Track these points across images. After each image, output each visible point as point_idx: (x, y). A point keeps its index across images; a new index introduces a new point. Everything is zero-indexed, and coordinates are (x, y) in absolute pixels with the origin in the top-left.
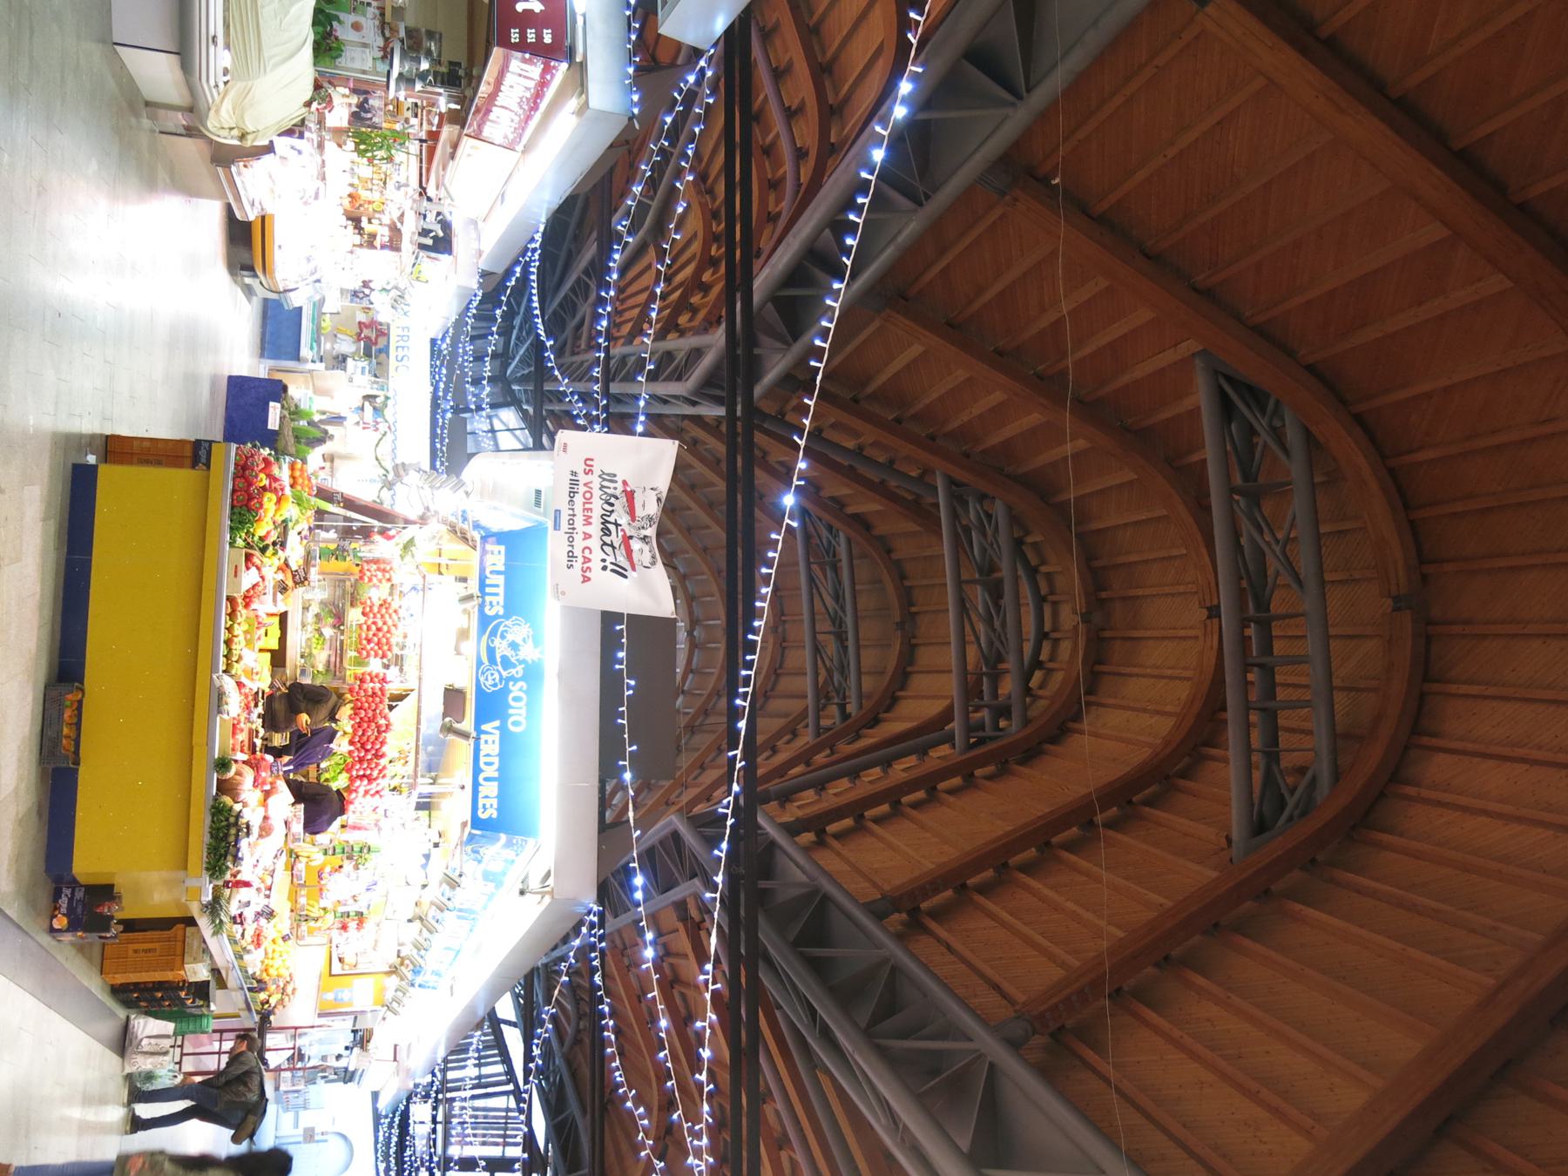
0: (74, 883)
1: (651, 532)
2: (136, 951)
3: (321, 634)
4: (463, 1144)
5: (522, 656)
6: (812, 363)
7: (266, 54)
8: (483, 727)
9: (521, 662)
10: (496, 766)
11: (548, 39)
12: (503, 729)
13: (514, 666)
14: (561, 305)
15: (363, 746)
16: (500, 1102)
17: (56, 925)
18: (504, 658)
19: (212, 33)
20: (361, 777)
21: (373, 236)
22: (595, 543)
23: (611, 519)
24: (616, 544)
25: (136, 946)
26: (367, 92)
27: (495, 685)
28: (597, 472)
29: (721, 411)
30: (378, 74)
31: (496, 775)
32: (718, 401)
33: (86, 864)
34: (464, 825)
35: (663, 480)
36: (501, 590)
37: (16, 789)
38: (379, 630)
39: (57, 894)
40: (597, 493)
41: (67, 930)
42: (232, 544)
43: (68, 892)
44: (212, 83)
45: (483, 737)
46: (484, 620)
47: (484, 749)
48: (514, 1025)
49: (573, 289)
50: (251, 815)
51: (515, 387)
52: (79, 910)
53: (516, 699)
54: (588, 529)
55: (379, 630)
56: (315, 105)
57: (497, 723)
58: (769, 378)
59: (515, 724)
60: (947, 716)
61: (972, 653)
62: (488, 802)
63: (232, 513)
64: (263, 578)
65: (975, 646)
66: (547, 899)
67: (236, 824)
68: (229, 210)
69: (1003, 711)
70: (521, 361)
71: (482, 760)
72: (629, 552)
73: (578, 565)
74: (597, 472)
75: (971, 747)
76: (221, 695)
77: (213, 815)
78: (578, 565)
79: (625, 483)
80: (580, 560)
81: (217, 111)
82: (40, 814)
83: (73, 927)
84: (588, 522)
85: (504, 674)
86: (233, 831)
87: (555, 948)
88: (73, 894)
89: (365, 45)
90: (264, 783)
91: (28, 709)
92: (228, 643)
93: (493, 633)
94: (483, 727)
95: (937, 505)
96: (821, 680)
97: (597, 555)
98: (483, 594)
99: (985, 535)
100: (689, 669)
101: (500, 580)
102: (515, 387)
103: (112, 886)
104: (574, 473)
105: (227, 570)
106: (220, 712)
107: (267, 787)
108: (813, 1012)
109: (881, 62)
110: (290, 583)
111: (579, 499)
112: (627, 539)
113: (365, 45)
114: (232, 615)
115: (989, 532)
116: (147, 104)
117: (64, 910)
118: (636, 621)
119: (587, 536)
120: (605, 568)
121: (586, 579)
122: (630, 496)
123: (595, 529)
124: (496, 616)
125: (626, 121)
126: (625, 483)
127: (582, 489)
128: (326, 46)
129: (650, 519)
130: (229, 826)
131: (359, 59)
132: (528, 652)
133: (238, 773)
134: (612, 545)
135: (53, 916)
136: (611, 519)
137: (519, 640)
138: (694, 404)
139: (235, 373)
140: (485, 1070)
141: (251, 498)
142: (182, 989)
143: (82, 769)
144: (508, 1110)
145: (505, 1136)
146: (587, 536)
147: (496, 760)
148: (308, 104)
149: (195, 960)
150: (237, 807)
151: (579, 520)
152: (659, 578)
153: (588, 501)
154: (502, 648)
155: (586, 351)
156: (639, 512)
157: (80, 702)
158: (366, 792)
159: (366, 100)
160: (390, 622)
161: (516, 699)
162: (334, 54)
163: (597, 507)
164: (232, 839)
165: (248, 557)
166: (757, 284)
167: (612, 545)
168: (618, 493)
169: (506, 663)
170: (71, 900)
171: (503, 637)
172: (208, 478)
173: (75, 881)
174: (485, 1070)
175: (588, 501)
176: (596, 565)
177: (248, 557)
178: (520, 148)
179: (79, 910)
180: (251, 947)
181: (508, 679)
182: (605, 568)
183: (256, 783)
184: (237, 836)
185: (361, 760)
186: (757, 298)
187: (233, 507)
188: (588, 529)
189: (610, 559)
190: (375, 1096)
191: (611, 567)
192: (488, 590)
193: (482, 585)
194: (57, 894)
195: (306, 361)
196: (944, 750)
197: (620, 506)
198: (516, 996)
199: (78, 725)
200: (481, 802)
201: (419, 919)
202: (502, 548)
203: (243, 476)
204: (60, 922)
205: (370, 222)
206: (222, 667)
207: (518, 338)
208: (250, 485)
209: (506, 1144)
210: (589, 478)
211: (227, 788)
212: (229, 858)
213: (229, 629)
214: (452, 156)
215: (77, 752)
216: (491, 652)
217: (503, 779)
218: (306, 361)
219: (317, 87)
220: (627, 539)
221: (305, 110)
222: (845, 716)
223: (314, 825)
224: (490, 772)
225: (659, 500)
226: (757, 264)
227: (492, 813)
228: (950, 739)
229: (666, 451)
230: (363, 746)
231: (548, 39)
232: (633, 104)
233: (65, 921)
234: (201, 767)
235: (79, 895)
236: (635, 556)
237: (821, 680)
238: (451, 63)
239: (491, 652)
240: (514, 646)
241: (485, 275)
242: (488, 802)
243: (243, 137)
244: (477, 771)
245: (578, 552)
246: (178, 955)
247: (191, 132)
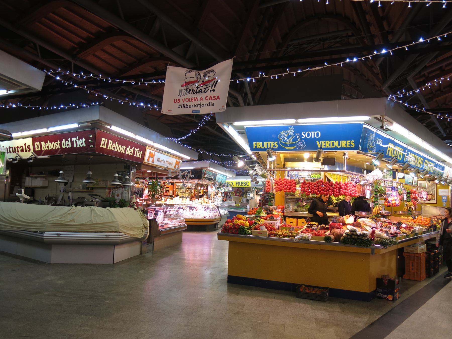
0: (375, 292)
1: (202, 73)
2: (412, 269)
3: (305, 205)
5: (292, 134)
7: (111, 221)
8: (319, 147)
9: (295, 134)
10: (334, 142)
11: (91, 136)
12: (320, 140)
15: (328, 190)
17: (392, 299)
18: (293, 141)
19: (105, 236)
20: (340, 191)
21: (204, 192)
22: (204, 95)
23: (195, 90)
24: (205, 87)
25: (411, 269)
27: (303, 143)
28: (179, 97)
30: (129, 189)
31: (337, 142)
33: (366, 287)
34: (358, 153)
35: (182, 71)
36: (269, 143)
37: (329, 312)
38: (286, 185)
39: (380, 298)
40: (186, 97)
41: (393, 295)
42: (250, 234)
43: (379, 294)
44: (121, 236)
45: (323, 147)
46: (280, 148)
50: (347, 229)
52: (386, 291)
54: (199, 99)
55: (286, 185)
56: (136, 207)
57: (318, 142)
59: (318, 134)
62: (348, 144)
63: (240, 234)
64: (264, 224)
66: (386, 117)
67: (350, 235)
68: (184, 231)
72: (209, 81)
73: (213, 102)
74: (179, 97)
76: (302, 239)
77: (346, 244)
78: (213, 102)
79: (182, 86)
80: (210, 101)
81: (133, 235)
82: (344, 303)
83: (392, 293)
84: (196, 99)
85: (299, 140)
86: (353, 237)
88: (380, 292)
89: (122, 193)
90: (339, 225)
91: (301, 305)
92: (284, 236)
93: (284, 145)
94: (319, 147)
97: (208, 94)
98: (268, 149)
101: (265, 143)
103: (378, 280)
104: (179, 106)
105: (260, 236)
106: (308, 240)
107: (341, 224)
109: (129, 40)
110: (270, 215)
111: (189, 104)
112: (204, 83)
113: (122, 193)
114: (275, 235)
116: (141, 254)
117: (385, 296)
118: (234, 75)
119: (201, 99)
120: (214, 90)
121: (218, 98)
122: (187, 83)
123: (199, 96)
124: (278, 144)
125: (102, 107)
126: (182, 86)
127: (185, 103)
128: (122, 204)
129: (197, 75)
130: (351, 238)
131: (126, 195)
132: (291, 132)
133: (333, 234)
134: (205, 89)
135: (388, 299)
136: (195, 90)
137: (286, 135)
141: (235, 228)
142: (430, 254)
143: (330, 287)
146: (201, 99)
147: (331, 142)
148: (136, 209)
149: (417, 249)
150: (344, 235)
151: (196, 103)
152: (218, 67)
153: (189, 100)
154: (289, 142)
156: (194, 79)
157: (306, 286)
158: (346, 189)
159: (136, 192)
160: (283, 182)
162: (123, 202)
163: (191, 96)
164: (356, 237)
165: (256, 229)
167: (205, 89)
168: (186, 88)
169: (295, 140)
170: (382, 293)
171: (286, 141)
173: (374, 291)
175: (189, 100)
176: (212, 94)
177: (256, 229)
179: (386, 291)
180: (412, 230)
181: (301, 139)
182: (214, 90)
183: (339, 228)
184: (355, 235)
185: (333, 191)
187: (238, 234)
188: (199, 99)
189: (210, 89)
191: (213, 88)
194: (380, 298)
195: (247, 211)
197: (190, 87)
199: (314, 287)
200: (348, 146)
201: (404, 169)
202: (254, 143)
203: (228, 230)
204: (390, 297)
205: (200, 193)
206: (293, 239)
208: (231, 228)
210: (181, 101)
211: (338, 237)
212: (363, 238)
213: (280, 236)
215: (324, 288)
216: (291, 145)
217: (339, 139)
218: (247, 211)
219: (131, 206)
220: (204, 83)
221: (138, 210)
222: (353, 35)
223: (368, 209)
224: (336, 143)
225: (190, 72)
227: (352, 142)
229: (171, 71)
230: (328, 190)
231: (91, 136)
232: (99, 104)
233: (390, 296)
234: (328, 247)
235: (380, 290)
236: (210, 79)
238: (124, 168)
239: (291, 145)
240: (289, 137)
242: (348, 144)
243: (146, 228)
244: (336, 148)
245: (207, 102)
246: (416, 256)
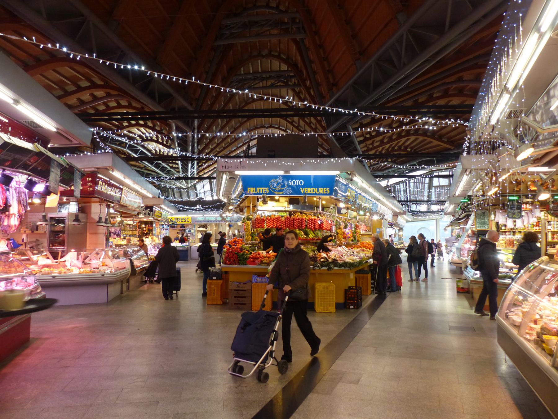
4: (423, 196)
6: (115, 67)
11: (90, 179)
14: (163, 172)
16: (412, 184)
18: (281, 187)
26: (110, 233)
29: (196, 120)
32: (193, 122)
36: (261, 189)
47: (309, 192)
48: (388, 181)
49: (158, 168)
53: (294, 183)
58: (185, 104)
59: (301, 183)
60: (295, 41)
61: (275, 32)
62: (325, 191)
65: (272, 31)
69: (293, 20)
71: (312, 193)
75: (305, 32)
93: (274, 190)
95: (223, 45)
96: (282, 84)
99: (233, 27)
100: (285, 131)
101: (258, 189)
108: (391, 87)
115: (232, 26)
124: (269, 189)
137: (276, 183)
138: (194, 128)
139: (181, 272)
140: (402, 189)
144: (414, 182)
145: (422, 183)
154: (278, 188)
166: (156, 110)
171: (275, 187)
172: (232, 272)
174: (402, 189)
178: (121, 187)
186: (161, 109)
190: (407, 222)
193: (260, 194)
196: (307, 42)
198: (380, 181)
209: (425, 183)
214: (126, 207)
216: (280, 191)
226: (147, 110)
228: (302, 40)
231: (90, 179)
237: (282, 84)
239: (280, 191)
240: (278, 184)
241: (10, 206)
242: (325, 191)
247: (128, 281)
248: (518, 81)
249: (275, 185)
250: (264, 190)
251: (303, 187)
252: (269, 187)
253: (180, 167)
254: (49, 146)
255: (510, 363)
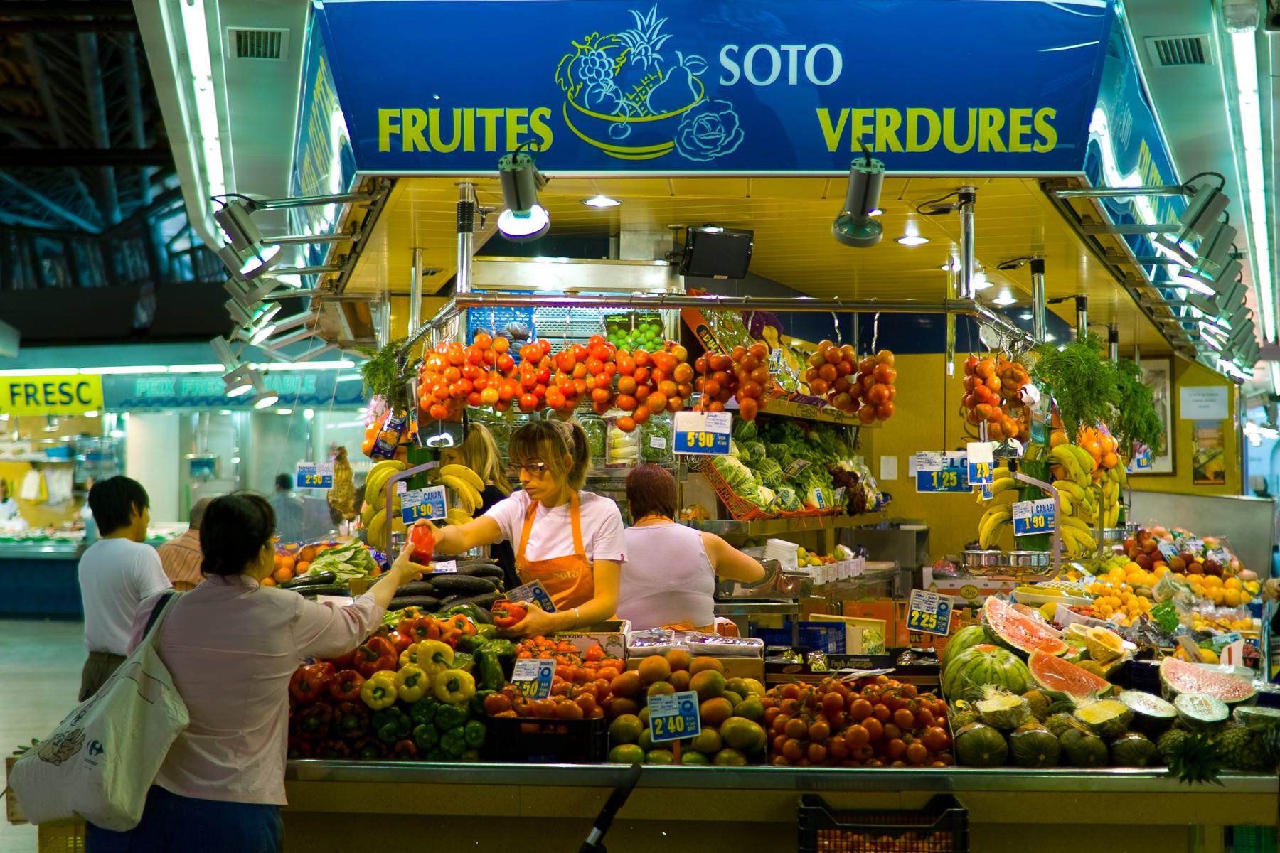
13: (680, 75)
18: (659, 102)
27: (728, 122)
36: (490, 115)
47: (886, 137)
51: (118, 217)
53: (762, 65)
57: (823, 114)
62: (1017, 129)
70: (74, 210)
71: (912, 146)
87: (90, 705)
93: (600, 130)
101: (465, 118)
102: (118, 217)
124: (554, 123)
137: (614, 65)
154: (632, 110)
155: (35, 93)
161: (762, 65)
169: (673, 94)
171: (608, 106)
192: (490, 145)
193: (480, 159)
207: (37, 217)
216: (644, 135)
224: (942, 125)
240: (628, 78)
248: (906, 522)
249: (608, 87)
250: (513, 129)
251: (836, 99)
252: (553, 98)
253: (51, 106)
254: (143, 316)
255: (375, 317)
